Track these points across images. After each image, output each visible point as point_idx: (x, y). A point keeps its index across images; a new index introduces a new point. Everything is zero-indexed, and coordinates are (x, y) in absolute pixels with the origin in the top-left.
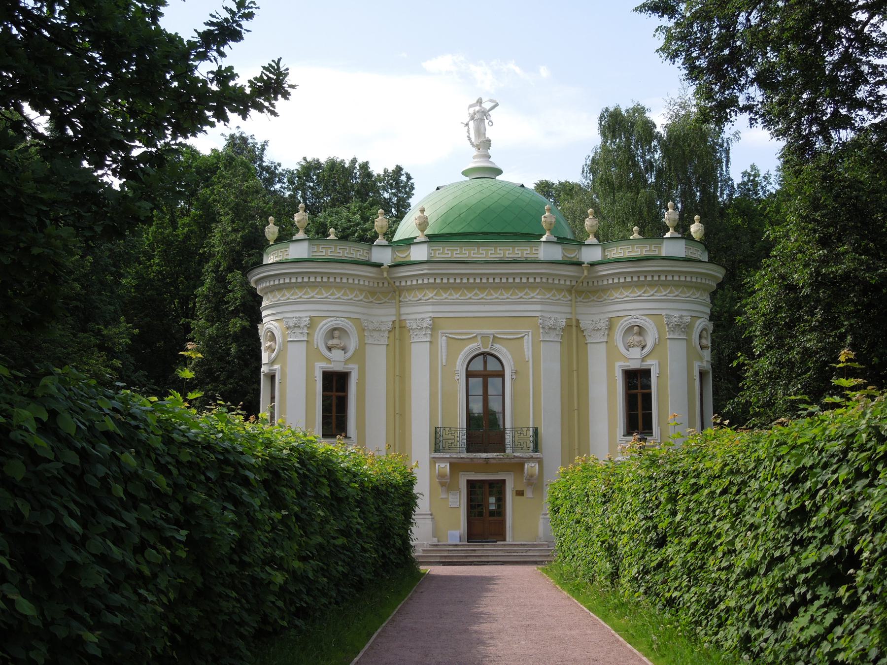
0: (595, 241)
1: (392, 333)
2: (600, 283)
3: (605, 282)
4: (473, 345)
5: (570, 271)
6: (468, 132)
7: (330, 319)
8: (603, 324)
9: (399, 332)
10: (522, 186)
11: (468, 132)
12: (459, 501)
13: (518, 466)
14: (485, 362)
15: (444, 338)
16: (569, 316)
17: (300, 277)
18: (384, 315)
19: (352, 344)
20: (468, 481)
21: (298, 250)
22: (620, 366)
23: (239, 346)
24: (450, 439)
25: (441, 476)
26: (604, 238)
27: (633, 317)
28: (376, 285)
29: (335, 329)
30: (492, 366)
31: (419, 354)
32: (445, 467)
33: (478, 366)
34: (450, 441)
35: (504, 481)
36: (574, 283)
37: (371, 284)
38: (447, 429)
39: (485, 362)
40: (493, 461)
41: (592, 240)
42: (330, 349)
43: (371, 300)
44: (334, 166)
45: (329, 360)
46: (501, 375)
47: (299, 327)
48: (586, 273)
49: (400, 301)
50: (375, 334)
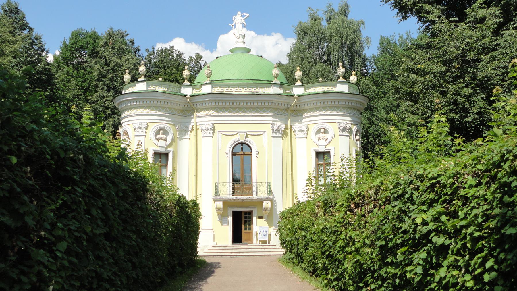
0: (300, 84)
15: (220, 134)
17: (145, 101)
21: (141, 87)
29: (161, 130)
32: (220, 204)
35: (252, 211)
41: (299, 83)
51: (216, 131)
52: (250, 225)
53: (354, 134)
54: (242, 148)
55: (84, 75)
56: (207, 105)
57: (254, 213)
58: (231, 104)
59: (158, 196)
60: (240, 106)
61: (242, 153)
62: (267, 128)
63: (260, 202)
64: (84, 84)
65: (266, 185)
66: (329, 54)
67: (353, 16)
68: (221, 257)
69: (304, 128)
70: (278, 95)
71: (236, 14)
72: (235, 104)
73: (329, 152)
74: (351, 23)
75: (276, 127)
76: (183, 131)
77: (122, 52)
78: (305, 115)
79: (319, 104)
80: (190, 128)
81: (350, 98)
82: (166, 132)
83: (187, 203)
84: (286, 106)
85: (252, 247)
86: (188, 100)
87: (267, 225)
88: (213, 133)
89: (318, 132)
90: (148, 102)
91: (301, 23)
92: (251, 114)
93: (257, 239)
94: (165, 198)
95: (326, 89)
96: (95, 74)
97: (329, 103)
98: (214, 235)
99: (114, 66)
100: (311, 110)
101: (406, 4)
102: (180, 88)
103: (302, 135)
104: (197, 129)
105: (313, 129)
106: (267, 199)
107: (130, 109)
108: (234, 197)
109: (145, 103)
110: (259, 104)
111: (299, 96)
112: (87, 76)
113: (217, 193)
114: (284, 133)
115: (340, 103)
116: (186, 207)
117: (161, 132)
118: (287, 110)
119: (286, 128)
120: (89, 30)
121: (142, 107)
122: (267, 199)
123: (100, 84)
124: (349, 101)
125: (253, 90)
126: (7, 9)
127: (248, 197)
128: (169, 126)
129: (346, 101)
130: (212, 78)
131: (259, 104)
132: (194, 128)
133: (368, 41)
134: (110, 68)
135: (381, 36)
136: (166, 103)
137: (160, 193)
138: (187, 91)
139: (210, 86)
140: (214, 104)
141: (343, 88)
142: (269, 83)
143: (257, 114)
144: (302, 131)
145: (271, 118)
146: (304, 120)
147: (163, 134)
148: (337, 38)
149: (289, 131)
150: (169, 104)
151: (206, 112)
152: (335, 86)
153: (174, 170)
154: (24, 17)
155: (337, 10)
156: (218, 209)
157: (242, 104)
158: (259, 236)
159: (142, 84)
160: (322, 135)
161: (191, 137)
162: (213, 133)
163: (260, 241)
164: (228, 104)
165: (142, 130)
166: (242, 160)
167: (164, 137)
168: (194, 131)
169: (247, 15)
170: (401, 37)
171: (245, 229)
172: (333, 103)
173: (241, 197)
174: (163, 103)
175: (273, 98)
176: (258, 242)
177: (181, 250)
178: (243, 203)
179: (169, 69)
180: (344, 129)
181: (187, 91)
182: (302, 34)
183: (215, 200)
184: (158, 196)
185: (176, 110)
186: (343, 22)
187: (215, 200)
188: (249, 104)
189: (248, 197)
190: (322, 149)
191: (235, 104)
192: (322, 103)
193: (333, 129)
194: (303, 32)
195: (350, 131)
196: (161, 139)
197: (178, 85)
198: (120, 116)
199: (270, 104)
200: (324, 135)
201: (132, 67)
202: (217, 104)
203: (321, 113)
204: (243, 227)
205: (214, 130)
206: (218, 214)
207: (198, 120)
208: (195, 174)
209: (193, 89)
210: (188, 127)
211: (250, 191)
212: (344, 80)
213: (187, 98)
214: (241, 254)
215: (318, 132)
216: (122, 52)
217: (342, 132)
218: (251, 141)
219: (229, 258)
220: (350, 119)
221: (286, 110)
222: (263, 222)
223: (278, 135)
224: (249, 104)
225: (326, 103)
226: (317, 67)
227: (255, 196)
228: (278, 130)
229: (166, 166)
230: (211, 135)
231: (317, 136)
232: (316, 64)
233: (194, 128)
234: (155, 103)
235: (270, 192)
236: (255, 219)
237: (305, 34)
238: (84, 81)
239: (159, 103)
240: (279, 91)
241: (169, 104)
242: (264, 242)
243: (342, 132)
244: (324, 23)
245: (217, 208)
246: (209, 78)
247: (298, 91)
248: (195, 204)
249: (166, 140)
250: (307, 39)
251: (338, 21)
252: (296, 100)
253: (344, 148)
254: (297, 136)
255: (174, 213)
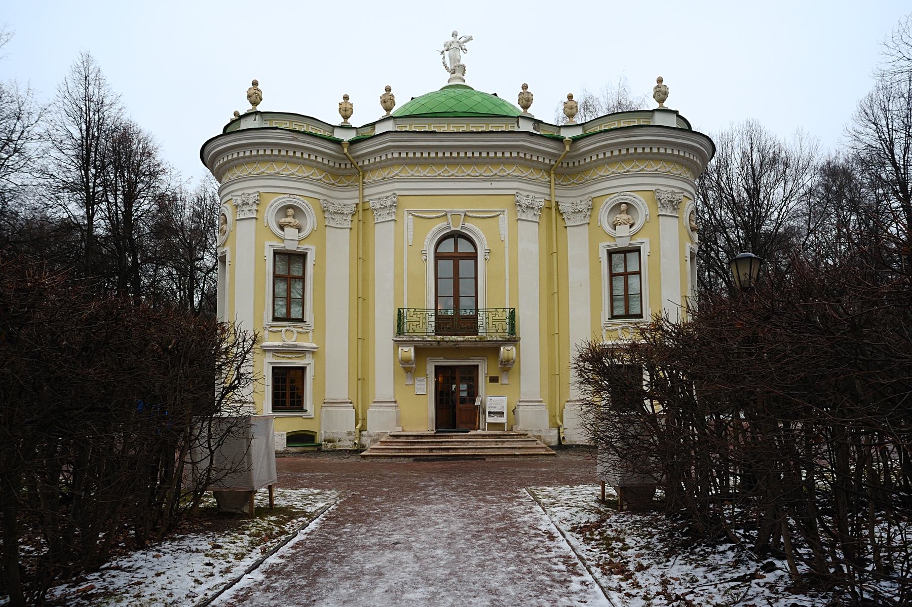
1: (356, 217)
2: (582, 163)
3: (588, 160)
4: (442, 224)
6: (444, 58)
7: (282, 196)
8: (583, 206)
9: (362, 212)
10: (495, 94)
11: (444, 58)
12: (425, 387)
13: (491, 350)
14: (456, 244)
15: (411, 216)
16: (547, 198)
18: (348, 198)
19: (310, 223)
20: (436, 367)
22: (605, 247)
23: (825, 493)
24: (415, 321)
25: (405, 362)
27: (620, 193)
28: (337, 166)
30: (464, 247)
31: (383, 235)
32: (409, 352)
33: (448, 247)
34: (415, 324)
36: (553, 163)
37: (331, 164)
38: (412, 311)
39: (456, 244)
40: (462, 345)
42: (282, 227)
43: (333, 182)
45: (283, 240)
46: (474, 257)
47: (247, 204)
48: (568, 148)
49: (364, 183)
50: (338, 217)
73: (638, 250)
113: (400, 330)
178: (456, 350)
183: (398, 344)
214: (452, 453)
218: (474, 228)
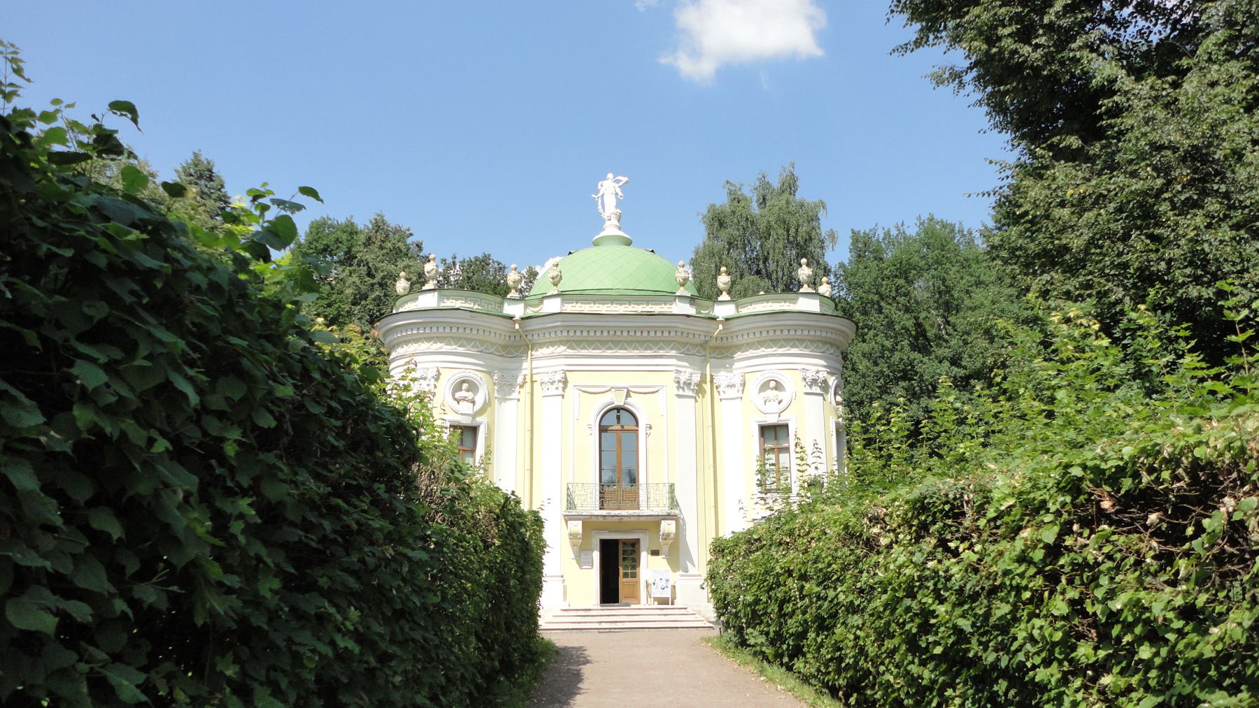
0: (728, 298)
5: (704, 326)
17: (434, 326)
21: (428, 300)
26: (738, 293)
29: (464, 381)
32: (577, 527)
35: (638, 540)
41: (725, 297)
44: (540, 588)
51: (570, 385)
52: (634, 567)
53: (832, 391)
54: (618, 418)
55: (329, 295)
56: (553, 335)
57: (644, 544)
58: (598, 334)
59: (452, 484)
60: (615, 338)
61: (618, 427)
62: (667, 380)
63: (655, 521)
64: (329, 310)
65: (666, 489)
66: (766, 259)
67: (806, 194)
68: (579, 634)
69: (737, 381)
70: (688, 316)
71: (605, 179)
72: (605, 334)
73: (786, 426)
74: (802, 206)
75: (683, 378)
76: (507, 385)
77: (397, 254)
78: (738, 355)
79: (765, 334)
80: (520, 380)
81: (823, 323)
82: (473, 387)
83: (521, 515)
84: (703, 338)
85: (638, 612)
86: (517, 326)
87: (668, 568)
88: (564, 389)
89: (765, 387)
90: (441, 330)
91: (713, 206)
92: (636, 352)
93: (649, 595)
94: (472, 494)
95: (777, 307)
96: (349, 291)
97: (786, 332)
98: (565, 587)
99: (383, 278)
100: (750, 346)
101: (1025, 61)
102: (502, 304)
103: (732, 393)
104: (532, 382)
105: (754, 382)
106: (668, 517)
107: (407, 342)
108: (604, 512)
109: (434, 330)
110: (652, 334)
111: (727, 319)
112: (334, 297)
113: (571, 504)
114: (699, 390)
115: (806, 333)
116: (522, 524)
117: (465, 386)
118: (703, 345)
119: (703, 380)
120: (342, 220)
121: (428, 339)
122: (668, 517)
123: (356, 309)
124: (821, 328)
125: (640, 308)
126: (192, 171)
127: (631, 512)
128: (480, 374)
129: (816, 328)
130: (563, 286)
131: (652, 334)
132: (528, 379)
133: (832, 236)
134: (375, 281)
135: (853, 232)
136: (474, 332)
137: (457, 474)
138: (515, 310)
139: (558, 300)
140: (565, 334)
141: (813, 305)
142: (671, 297)
143: (648, 353)
144: (733, 386)
145: (674, 361)
146: (736, 365)
147: (468, 390)
148: (781, 231)
149: (707, 387)
150: (481, 332)
151: (551, 349)
152: (794, 301)
153: (488, 452)
154: (222, 186)
155: (776, 184)
156: (573, 536)
157: (618, 333)
158: (653, 588)
159: (430, 295)
160: (771, 393)
161: (521, 397)
162: (564, 389)
163: (655, 599)
164: (592, 334)
165: (427, 382)
166: (619, 441)
167: (470, 395)
168: (528, 386)
169: (624, 179)
170: (887, 234)
171: (626, 575)
172: (792, 332)
173: (617, 512)
174: (468, 331)
175: (681, 325)
176: (651, 601)
177: (508, 629)
178: (621, 524)
179: (482, 279)
180: (814, 382)
181: (515, 310)
182: (716, 224)
183: (568, 518)
184: (452, 484)
185: (493, 344)
186: (788, 202)
187: (568, 518)
188: (632, 333)
189: (631, 512)
190: (772, 420)
191: (605, 334)
192: (771, 333)
193: (794, 382)
194: (718, 221)
195: (825, 386)
196: (464, 399)
197: (499, 299)
198: (389, 354)
199: (673, 334)
200: (775, 392)
201: (414, 279)
202: (571, 333)
203: (769, 351)
204: (621, 571)
205: (565, 382)
206: (573, 545)
207: (535, 364)
208: (528, 466)
209: (526, 307)
210: (516, 378)
211: (634, 501)
212: (810, 290)
213: (515, 322)
214: (619, 625)
215: (765, 387)
216: (397, 254)
217: (811, 386)
218: (635, 403)
219: (595, 634)
220: (823, 363)
221: (701, 345)
222: (660, 562)
223: (688, 392)
224: (632, 333)
225: (778, 333)
226: (745, 280)
227: (644, 510)
228: (688, 384)
229: (473, 451)
230: (560, 391)
231: (763, 394)
232: (742, 276)
233: (528, 379)
234: (454, 330)
235: (674, 503)
236: (644, 556)
237: (722, 224)
238: (329, 305)
239: (461, 330)
240: (691, 311)
241: (481, 332)
242: (663, 601)
243: (811, 386)
244: (755, 209)
245: (571, 534)
246: (556, 285)
247: (723, 310)
248: (538, 522)
249: (473, 402)
250: (724, 234)
251: (776, 203)
252: (721, 327)
253: (815, 421)
254: (723, 396)
255: (493, 537)
